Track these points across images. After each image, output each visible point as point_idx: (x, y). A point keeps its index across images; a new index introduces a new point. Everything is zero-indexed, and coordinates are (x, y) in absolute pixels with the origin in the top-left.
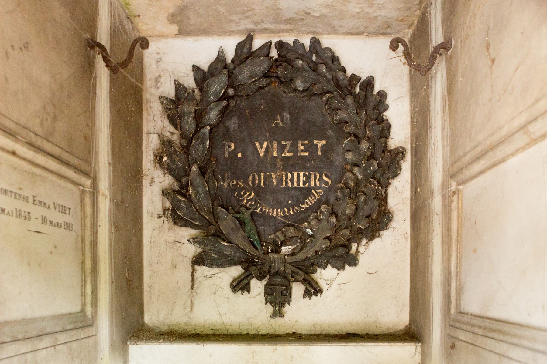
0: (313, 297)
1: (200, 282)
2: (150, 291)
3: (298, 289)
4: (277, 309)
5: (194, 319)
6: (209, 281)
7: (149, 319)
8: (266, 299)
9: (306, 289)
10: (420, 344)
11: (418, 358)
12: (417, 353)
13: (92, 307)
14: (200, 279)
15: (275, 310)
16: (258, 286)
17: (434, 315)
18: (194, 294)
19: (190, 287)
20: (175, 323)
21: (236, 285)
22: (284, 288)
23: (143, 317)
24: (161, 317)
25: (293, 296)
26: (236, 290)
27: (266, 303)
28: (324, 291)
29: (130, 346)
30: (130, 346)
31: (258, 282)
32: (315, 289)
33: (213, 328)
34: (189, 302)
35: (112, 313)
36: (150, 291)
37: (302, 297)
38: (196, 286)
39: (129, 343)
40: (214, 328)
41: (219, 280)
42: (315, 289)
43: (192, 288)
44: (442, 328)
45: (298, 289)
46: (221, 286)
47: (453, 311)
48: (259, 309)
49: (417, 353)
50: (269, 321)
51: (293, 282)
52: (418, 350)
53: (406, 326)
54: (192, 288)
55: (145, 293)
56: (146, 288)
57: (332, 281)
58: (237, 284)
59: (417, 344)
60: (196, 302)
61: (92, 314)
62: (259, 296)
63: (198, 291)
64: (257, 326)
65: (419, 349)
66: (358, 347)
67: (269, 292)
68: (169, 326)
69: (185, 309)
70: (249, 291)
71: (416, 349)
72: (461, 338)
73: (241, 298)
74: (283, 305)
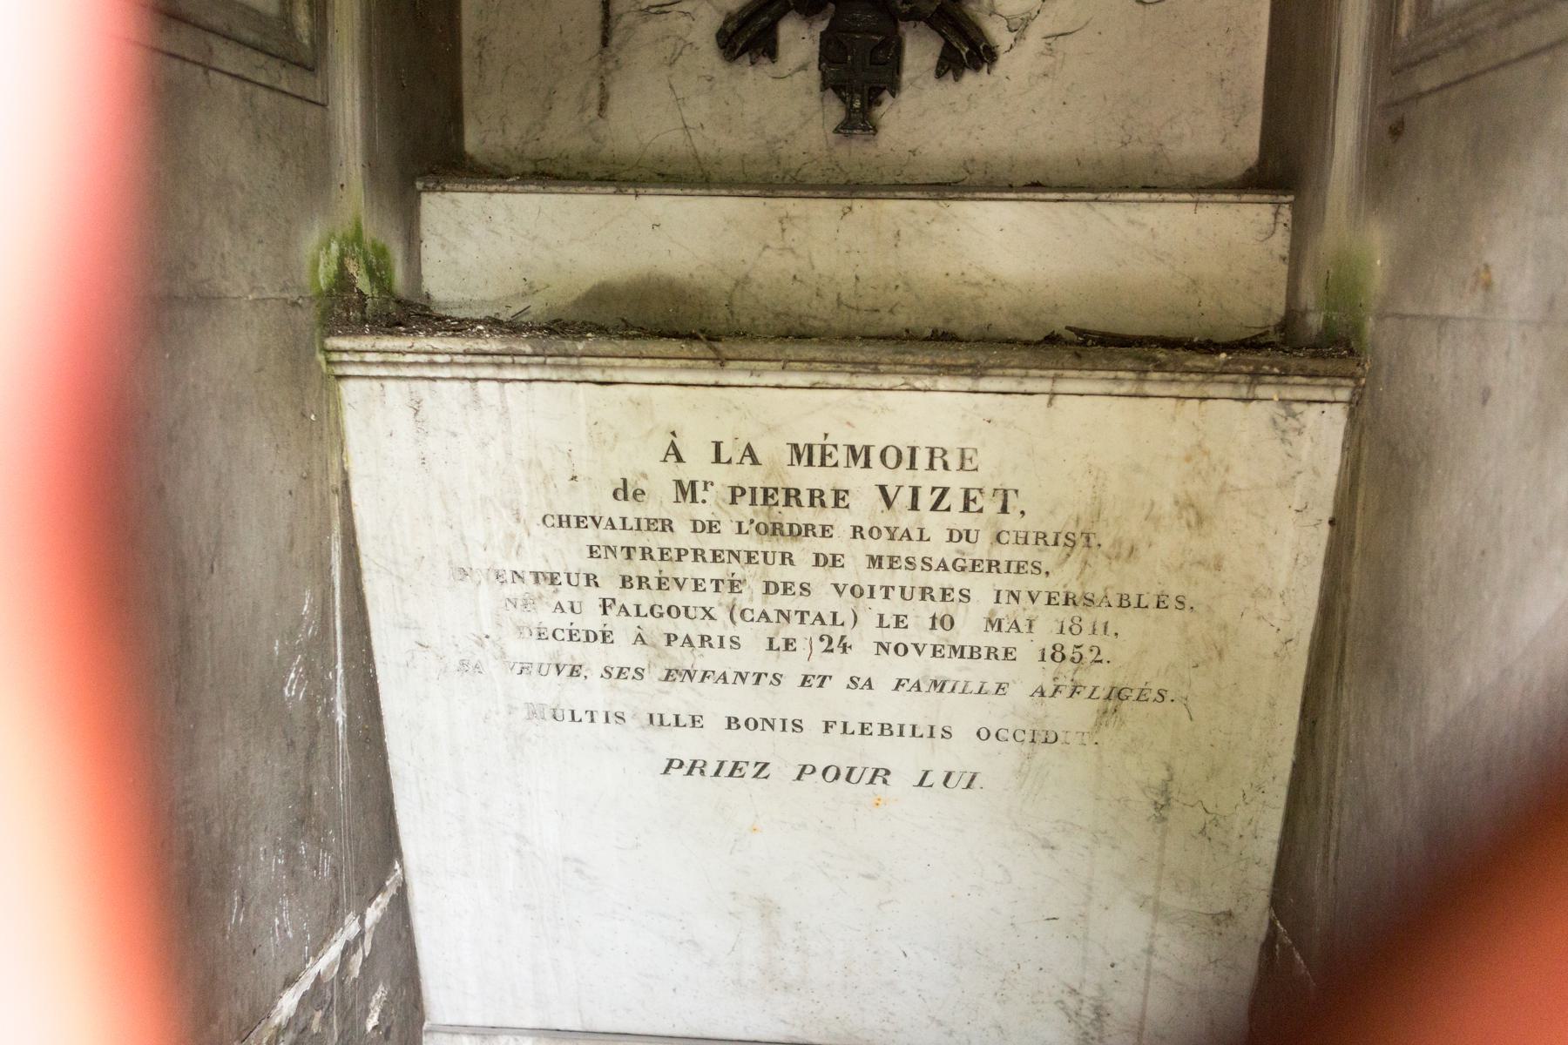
0: (969, 78)
1: (630, 28)
2: (480, 56)
3: (919, 51)
4: (857, 104)
5: (609, 143)
6: (653, 27)
7: (473, 141)
8: (824, 75)
9: (948, 46)
10: (1291, 198)
11: (1281, 242)
12: (1280, 227)
13: (311, 15)
14: (627, 19)
15: (850, 111)
16: (799, 40)
17: (1344, 74)
18: (610, 65)
19: (598, 42)
20: (554, 155)
21: (734, 33)
22: (879, 39)
23: (460, 133)
24: (514, 136)
25: (906, 76)
26: (733, 49)
27: (824, 87)
28: (1002, 49)
29: (425, 197)
30: (425, 197)
31: (803, 30)
32: (973, 46)
33: (664, 170)
34: (594, 92)
35: (370, 70)
36: (480, 56)
37: (933, 72)
38: (615, 40)
39: (419, 185)
40: (669, 171)
41: (684, 21)
42: (973, 46)
43: (605, 41)
44: (1365, 104)
45: (919, 51)
46: (690, 39)
47: (1405, 25)
48: (803, 114)
49: (1280, 227)
50: (830, 149)
51: (907, 17)
52: (1282, 219)
53: (1250, 170)
54: (605, 41)
55: (466, 64)
56: (467, 44)
57: (1027, 21)
58: (739, 29)
59: (1282, 198)
60: (616, 89)
61: (312, 33)
62: (802, 74)
63: (622, 56)
64: (795, 165)
65: (1286, 212)
66: (1097, 205)
67: (831, 52)
68: (535, 162)
69: (583, 110)
70: (772, 54)
71: (1276, 214)
72: (1425, 86)
73: (752, 79)
74: (872, 99)
